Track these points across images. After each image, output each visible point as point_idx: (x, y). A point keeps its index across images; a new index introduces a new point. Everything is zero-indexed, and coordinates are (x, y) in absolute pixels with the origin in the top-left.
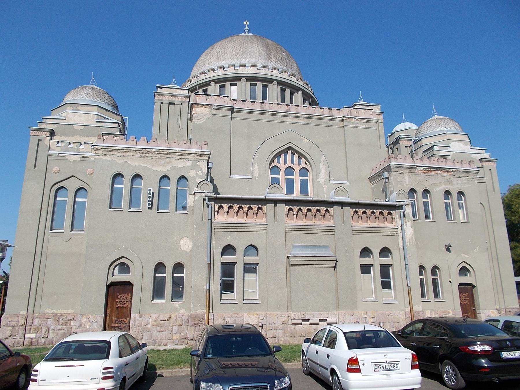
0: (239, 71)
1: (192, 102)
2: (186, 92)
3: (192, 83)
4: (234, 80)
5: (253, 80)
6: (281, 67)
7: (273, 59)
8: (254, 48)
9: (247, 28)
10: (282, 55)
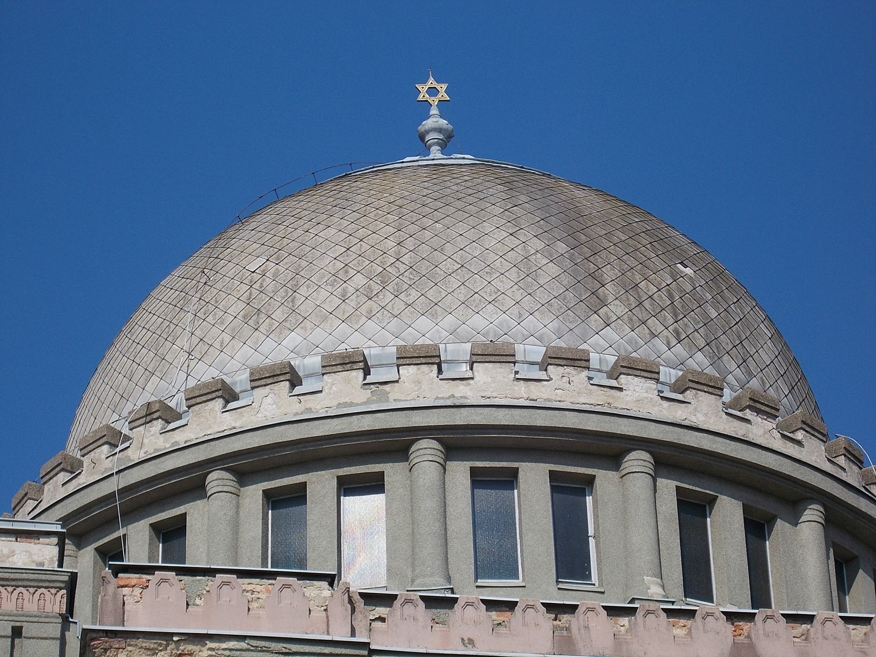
0: (397, 397)
1: (84, 619)
2: (45, 553)
3: (83, 479)
4: (365, 456)
5: (488, 450)
6: (672, 357)
7: (617, 308)
8: (489, 242)
9: (435, 121)
10: (675, 276)
